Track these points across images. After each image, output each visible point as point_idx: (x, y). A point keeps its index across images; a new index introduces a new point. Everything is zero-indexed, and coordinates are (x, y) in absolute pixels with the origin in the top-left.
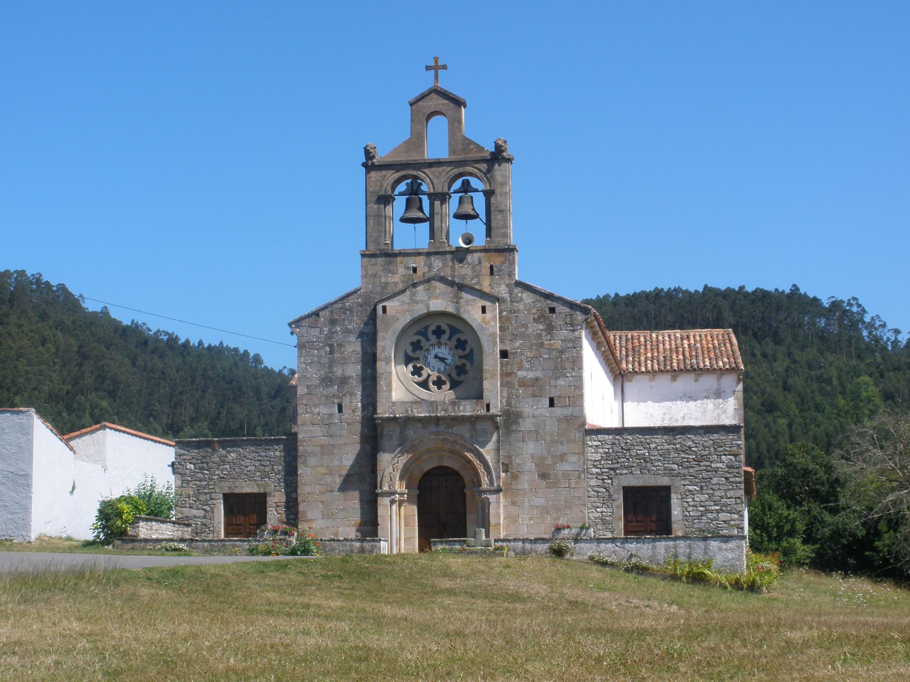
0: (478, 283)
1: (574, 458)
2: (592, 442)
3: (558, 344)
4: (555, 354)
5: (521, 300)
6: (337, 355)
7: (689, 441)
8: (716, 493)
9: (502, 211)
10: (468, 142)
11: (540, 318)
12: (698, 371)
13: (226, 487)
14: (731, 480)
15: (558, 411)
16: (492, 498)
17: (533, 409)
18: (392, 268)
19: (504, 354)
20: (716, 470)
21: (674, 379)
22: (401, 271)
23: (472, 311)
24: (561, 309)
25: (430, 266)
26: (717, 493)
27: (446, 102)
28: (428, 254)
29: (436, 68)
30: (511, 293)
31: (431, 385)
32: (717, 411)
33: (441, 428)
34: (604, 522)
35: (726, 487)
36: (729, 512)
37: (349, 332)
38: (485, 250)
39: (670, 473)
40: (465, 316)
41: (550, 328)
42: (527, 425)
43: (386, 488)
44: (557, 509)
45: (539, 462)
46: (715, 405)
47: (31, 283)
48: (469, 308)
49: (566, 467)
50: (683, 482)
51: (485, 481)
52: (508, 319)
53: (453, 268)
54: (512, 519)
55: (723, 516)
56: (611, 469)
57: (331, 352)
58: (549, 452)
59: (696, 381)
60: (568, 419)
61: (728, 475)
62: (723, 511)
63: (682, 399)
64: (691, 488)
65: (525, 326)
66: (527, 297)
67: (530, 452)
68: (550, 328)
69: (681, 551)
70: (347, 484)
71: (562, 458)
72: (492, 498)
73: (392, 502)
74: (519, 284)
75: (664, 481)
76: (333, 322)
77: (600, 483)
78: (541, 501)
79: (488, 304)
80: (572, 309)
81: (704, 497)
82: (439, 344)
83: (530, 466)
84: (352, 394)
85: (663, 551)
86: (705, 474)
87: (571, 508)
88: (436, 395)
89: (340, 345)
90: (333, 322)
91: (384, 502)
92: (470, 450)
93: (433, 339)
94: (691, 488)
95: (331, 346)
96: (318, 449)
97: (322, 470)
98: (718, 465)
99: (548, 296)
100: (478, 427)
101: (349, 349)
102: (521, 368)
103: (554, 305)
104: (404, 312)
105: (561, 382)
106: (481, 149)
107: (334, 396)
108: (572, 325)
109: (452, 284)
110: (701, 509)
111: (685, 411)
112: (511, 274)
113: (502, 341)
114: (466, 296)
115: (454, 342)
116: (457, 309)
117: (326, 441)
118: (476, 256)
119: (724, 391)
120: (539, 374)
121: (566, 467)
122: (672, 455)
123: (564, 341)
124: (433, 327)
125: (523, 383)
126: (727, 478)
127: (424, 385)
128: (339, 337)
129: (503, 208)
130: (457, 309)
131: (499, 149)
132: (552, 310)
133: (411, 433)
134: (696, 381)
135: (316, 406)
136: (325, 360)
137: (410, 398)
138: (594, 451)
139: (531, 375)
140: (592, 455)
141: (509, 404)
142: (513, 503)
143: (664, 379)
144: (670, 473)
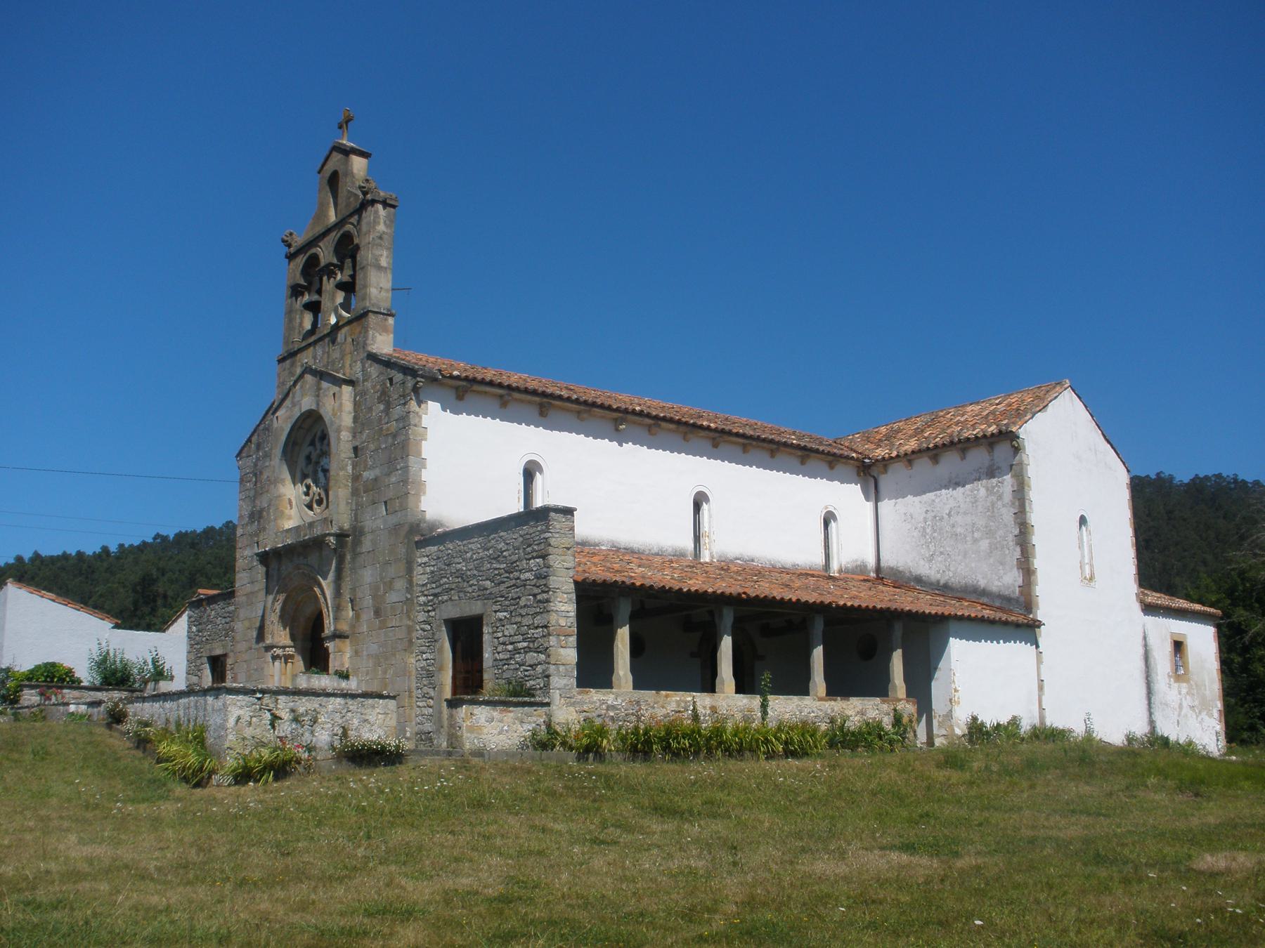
4: (390, 440)
14: (539, 597)
17: (376, 520)
24: (398, 377)
31: (315, 506)
32: (990, 498)
39: (484, 595)
42: (367, 544)
46: (987, 490)
47: (1229, 483)
50: (496, 608)
55: (531, 657)
56: (435, 595)
59: (963, 458)
61: (536, 591)
63: (946, 487)
64: (501, 615)
65: (370, 409)
66: (374, 370)
72: (330, 645)
73: (275, 658)
74: (373, 357)
75: (475, 608)
80: (405, 374)
83: (368, 601)
89: (261, 473)
94: (501, 615)
98: (528, 575)
110: (510, 647)
111: (952, 503)
114: (325, 385)
118: (344, 330)
119: (999, 468)
126: (535, 596)
132: (391, 380)
134: (963, 458)
143: (923, 464)
144: (484, 595)
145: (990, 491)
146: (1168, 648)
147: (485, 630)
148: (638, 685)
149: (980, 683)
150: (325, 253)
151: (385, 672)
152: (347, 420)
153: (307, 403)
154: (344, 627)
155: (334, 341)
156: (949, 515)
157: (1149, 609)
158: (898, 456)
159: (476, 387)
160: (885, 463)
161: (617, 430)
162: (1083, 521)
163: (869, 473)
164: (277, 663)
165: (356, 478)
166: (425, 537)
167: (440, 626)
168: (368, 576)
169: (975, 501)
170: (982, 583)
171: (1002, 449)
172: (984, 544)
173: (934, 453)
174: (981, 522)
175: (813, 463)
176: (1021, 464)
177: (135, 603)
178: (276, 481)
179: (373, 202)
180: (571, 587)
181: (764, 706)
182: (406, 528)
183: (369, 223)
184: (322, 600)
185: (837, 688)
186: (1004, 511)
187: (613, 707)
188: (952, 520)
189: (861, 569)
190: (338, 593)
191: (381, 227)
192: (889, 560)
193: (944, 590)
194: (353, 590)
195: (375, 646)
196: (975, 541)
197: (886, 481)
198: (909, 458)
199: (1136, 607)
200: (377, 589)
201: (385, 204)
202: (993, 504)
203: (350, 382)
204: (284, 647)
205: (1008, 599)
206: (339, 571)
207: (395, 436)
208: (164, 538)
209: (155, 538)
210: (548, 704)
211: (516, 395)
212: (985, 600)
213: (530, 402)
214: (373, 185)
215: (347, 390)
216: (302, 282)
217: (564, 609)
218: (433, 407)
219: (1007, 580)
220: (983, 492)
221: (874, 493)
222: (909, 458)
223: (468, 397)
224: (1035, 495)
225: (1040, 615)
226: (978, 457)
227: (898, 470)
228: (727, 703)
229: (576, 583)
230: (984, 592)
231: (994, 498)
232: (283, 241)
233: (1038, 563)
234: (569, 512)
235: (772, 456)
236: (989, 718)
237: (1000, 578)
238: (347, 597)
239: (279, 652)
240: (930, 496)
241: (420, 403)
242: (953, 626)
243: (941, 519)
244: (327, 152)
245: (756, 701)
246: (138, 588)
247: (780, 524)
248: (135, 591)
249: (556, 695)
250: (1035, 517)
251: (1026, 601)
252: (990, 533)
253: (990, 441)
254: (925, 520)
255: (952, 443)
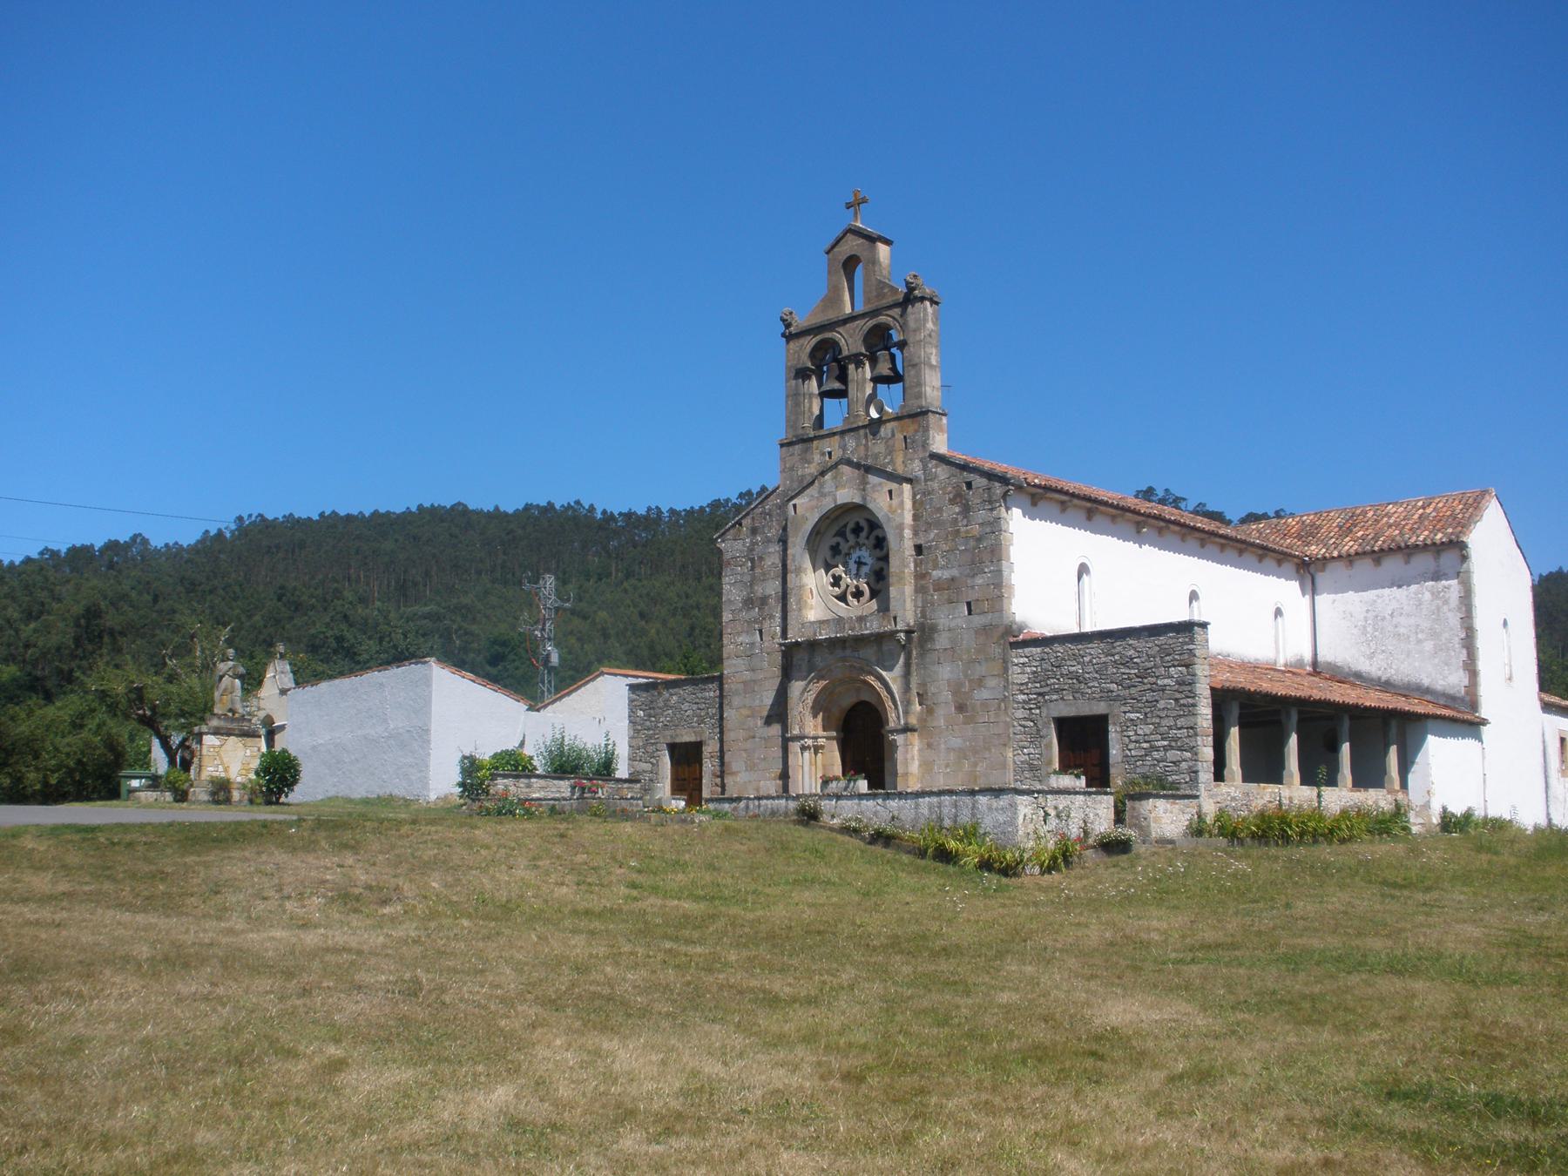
0: (892, 462)
1: (992, 682)
2: (1018, 657)
3: (976, 529)
4: (972, 543)
5: (936, 476)
6: (758, 571)
7: (1129, 649)
8: (1164, 722)
9: (914, 366)
10: (882, 285)
11: (955, 496)
12: (1408, 551)
13: (668, 736)
15: (978, 620)
16: (899, 739)
17: (952, 620)
18: (808, 456)
19: (919, 549)
20: (1163, 689)
21: (1377, 562)
22: (817, 458)
23: (880, 503)
24: (979, 482)
25: (844, 448)
26: (1165, 722)
27: (862, 240)
28: (843, 433)
29: (855, 204)
30: (925, 468)
31: (850, 598)
33: (848, 652)
34: (1032, 768)
35: (1175, 713)
36: (1180, 749)
37: (768, 541)
38: (898, 418)
39: (1108, 696)
40: (871, 506)
41: (966, 510)
42: (942, 641)
43: (796, 732)
44: (975, 752)
45: (956, 689)
48: (876, 495)
49: (985, 694)
50: (1124, 709)
51: (892, 716)
52: (922, 503)
53: (866, 446)
54: (927, 765)
55: (1173, 755)
56: (1039, 694)
57: (753, 568)
58: (966, 676)
59: (1407, 562)
60: (986, 630)
61: (1178, 696)
62: (1172, 748)
64: (1132, 716)
65: (940, 510)
66: (942, 472)
67: (946, 676)
68: (966, 510)
69: (945, 811)
70: (768, 721)
71: (980, 682)
72: (899, 739)
73: (803, 748)
74: (934, 456)
75: (1100, 708)
76: (754, 531)
77: (1026, 714)
78: (956, 742)
79: (894, 486)
81: (1149, 729)
82: (858, 545)
83: (946, 695)
84: (772, 617)
85: (926, 812)
86: (1149, 696)
87: (989, 749)
88: (853, 609)
89: (761, 559)
90: (754, 531)
91: (795, 747)
92: (870, 673)
93: (851, 537)
94: (1132, 716)
95: (752, 561)
96: (741, 686)
97: (745, 712)
98: (1166, 681)
99: (964, 467)
100: (885, 648)
101: (768, 562)
102: (935, 567)
103: (971, 477)
104: (812, 508)
105: (979, 581)
106: (894, 290)
107: (756, 621)
108: (990, 502)
109: (857, 466)
110: (1145, 745)
111: (1394, 605)
112: (925, 445)
113: (916, 533)
115: (872, 541)
116: (864, 499)
117: (748, 675)
118: (890, 426)
120: (955, 572)
121: (985, 694)
122: (1111, 670)
123: (981, 525)
124: (851, 525)
125: (939, 586)
126: (1176, 700)
127: (842, 598)
128: (758, 549)
129: (916, 360)
130: (864, 499)
131: (911, 289)
132: (969, 485)
133: (818, 661)
134: (1407, 562)
135: (739, 634)
136: (747, 578)
137: (829, 616)
138: (1021, 667)
139: (946, 574)
140: (1018, 676)
141: (924, 615)
142: (929, 746)
143: (1365, 565)
144: (1108, 696)
145: (1435, 595)
146: (1558, 744)
147: (1111, 728)
148: (1246, 779)
149: (1449, 778)
150: (850, 341)
151: (975, 765)
152: (908, 518)
153: (846, 495)
154: (913, 721)
155: (874, 434)
156: (1392, 615)
157: (1547, 707)
158: (1340, 556)
159: (1050, 495)
160: (1324, 561)
161: (1139, 532)
162: (1505, 623)
163: (1307, 571)
164: (806, 754)
165: (920, 576)
166: (1016, 640)
167: (1046, 725)
168: (945, 673)
169: (1420, 604)
170: (1426, 682)
171: (1448, 558)
172: (1429, 646)
173: (1377, 556)
174: (1425, 624)
175: (1269, 562)
176: (1468, 572)
177: (77, 640)
178: (799, 570)
179: (922, 299)
180: (1208, 693)
181: (1319, 796)
182: (1001, 629)
183: (917, 320)
184: (884, 693)
185: (1360, 782)
186: (1450, 615)
187: (1233, 799)
188: (1395, 621)
189: (1300, 663)
190: (907, 688)
191: (930, 325)
192: (1325, 655)
193: (1386, 686)
194: (923, 685)
195: (959, 741)
196: (1419, 642)
197: (1321, 578)
198: (1349, 559)
199: (1538, 704)
200: (961, 685)
201: (933, 302)
202: (1438, 609)
203: (910, 481)
204: (815, 738)
205: (1453, 698)
206: (907, 665)
207: (979, 540)
208: (54, 554)
209: (41, 553)
210: (1197, 797)
211: (1076, 501)
212: (1429, 698)
213: (1080, 507)
214: (920, 282)
215: (907, 487)
216: (809, 365)
217: (1205, 711)
218: (1016, 512)
219: (1452, 680)
220: (1427, 596)
221: (1311, 588)
222: (1349, 559)
223: (1042, 504)
224: (1478, 601)
225: (1484, 713)
226: (1423, 562)
227: (1338, 569)
228: (1293, 793)
229: (1212, 689)
230: (1428, 691)
231: (1440, 602)
232: (783, 320)
233: (1482, 665)
234: (1204, 625)
235: (1260, 561)
236: (1457, 809)
237: (1444, 678)
238: (914, 692)
239: (810, 742)
240: (1371, 594)
241: (1008, 509)
242: (1430, 724)
243: (1383, 619)
244: (838, 232)
245: (1315, 791)
246: (83, 621)
247: (1258, 623)
248: (78, 625)
249: (1202, 786)
250: (1480, 622)
251: (1471, 700)
252: (1434, 634)
253: (1437, 549)
254: (1366, 619)
255: (1399, 548)
